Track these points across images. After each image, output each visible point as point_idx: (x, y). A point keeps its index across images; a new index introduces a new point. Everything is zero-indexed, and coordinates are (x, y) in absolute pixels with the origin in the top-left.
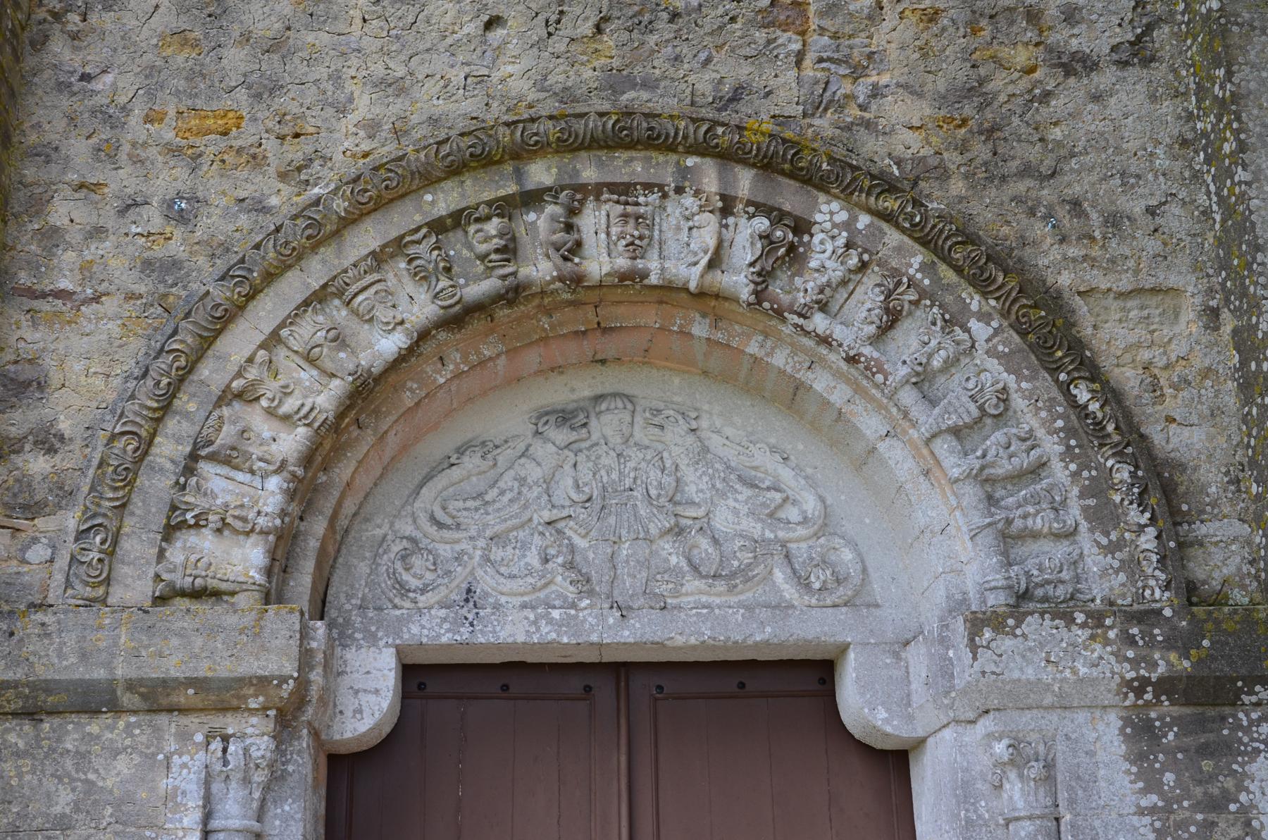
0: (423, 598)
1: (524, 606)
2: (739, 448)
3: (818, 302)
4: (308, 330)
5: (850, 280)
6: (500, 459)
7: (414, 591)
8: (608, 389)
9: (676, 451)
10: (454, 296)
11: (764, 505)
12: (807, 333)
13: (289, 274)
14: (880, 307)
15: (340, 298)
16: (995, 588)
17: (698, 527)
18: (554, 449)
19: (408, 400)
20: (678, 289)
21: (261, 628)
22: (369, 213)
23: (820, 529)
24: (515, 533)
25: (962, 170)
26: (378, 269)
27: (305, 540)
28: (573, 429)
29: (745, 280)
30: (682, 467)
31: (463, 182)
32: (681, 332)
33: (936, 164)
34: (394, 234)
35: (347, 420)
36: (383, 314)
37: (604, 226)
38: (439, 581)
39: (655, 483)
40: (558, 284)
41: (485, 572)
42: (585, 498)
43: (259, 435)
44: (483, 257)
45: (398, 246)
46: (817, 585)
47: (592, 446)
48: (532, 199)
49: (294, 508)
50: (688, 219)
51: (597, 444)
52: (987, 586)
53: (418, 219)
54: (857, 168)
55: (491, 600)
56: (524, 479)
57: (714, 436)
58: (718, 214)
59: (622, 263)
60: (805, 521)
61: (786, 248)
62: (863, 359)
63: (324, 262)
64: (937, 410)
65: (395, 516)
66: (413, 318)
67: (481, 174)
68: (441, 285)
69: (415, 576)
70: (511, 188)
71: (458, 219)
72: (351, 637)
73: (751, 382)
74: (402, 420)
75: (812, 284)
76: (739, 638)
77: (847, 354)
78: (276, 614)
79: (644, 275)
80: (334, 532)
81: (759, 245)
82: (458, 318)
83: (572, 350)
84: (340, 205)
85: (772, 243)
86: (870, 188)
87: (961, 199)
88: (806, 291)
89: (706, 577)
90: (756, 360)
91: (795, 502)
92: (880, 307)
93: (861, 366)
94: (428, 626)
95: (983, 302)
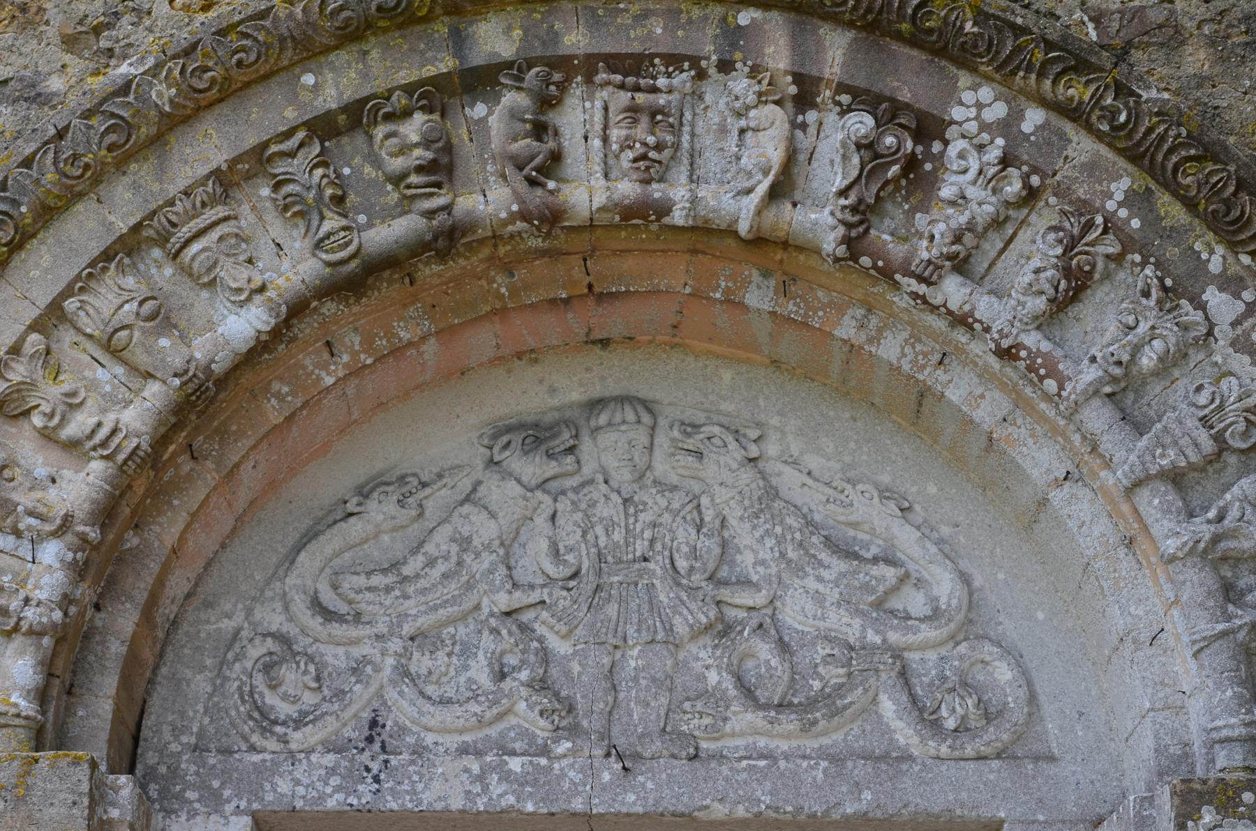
0: (297, 735)
1: (463, 750)
2: (827, 490)
3: (951, 257)
4: (110, 301)
5: (1007, 218)
6: (429, 504)
7: (284, 723)
8: (612, 388)
9: (722, 495)
10: (347, 244)
11: (866, 588)
12: (934, 309)
13: (80, 207)
14: (1056, 267)
15: (162, 247)
16: (1228, 740)
17: (754, 622)
18: (518, 489)
19: (273, 412)
20: (720, 232)
21: (28, 788)
22: (211, 105)
23: (959, 630)
24: (452, 630)
25: (1206, 30)
26: (225, 198)
27: (103, 642)
28: (550, 456)
29: (830, 221)
30: (732, 521)
31: (366, 53)
32: (728, 301)
33: (1161, 19)
34: (251, 141)
35: (172, 448)
36: (234, 274)
37: (598, 127)
38: (326, 707)
39: (685, 549)
40: (520, 225)
41: (401, 693)
42: (568, 572)
43: (28, 473)
44: (398, 179)
45: (258, 160)
46: (951, 724)
47: (583, 485)
48: (481, 81)
49: (85, 592)
50: (739, 115)
51: (591, 482)
52: (1215, 735)
53: (291, 115)
54: (1024, 30)
55: (410, 740)
56: (469, 540)
57: (788, 470)
58: (789, 105)
59: (627, 189)
60: (935, 616)
61: (902, 167)
62: (1023, 354)
63: (136, 187)
64: (1143, 442)
65: (254, 599)
66: (280, 281)
67: (395, 39)
68: (327, 226)
69: (285, 697)
70: (445, 64)
71: (357, 116)
72: (179, 797)
73: (848, 382)
74: (264, 445)
75: (942, 226)
76: (818, 809)
77: (998, 345)
78: (52, 766)
79: (664, 209)
80: (154, 627)
81: (856, 160)
82: (355, 281)
83: (550, 327)
84: (162, 94)
85: (877, 156)
86: (1045, 64)
87: (1201, 81)
88: (932, 237)
89: (765, 707)
90: (852, 348)
91: (919, 583)
92: (1056, 267)
93: (1022, 365)
94: (305, 781)
95: (1230, 260)
